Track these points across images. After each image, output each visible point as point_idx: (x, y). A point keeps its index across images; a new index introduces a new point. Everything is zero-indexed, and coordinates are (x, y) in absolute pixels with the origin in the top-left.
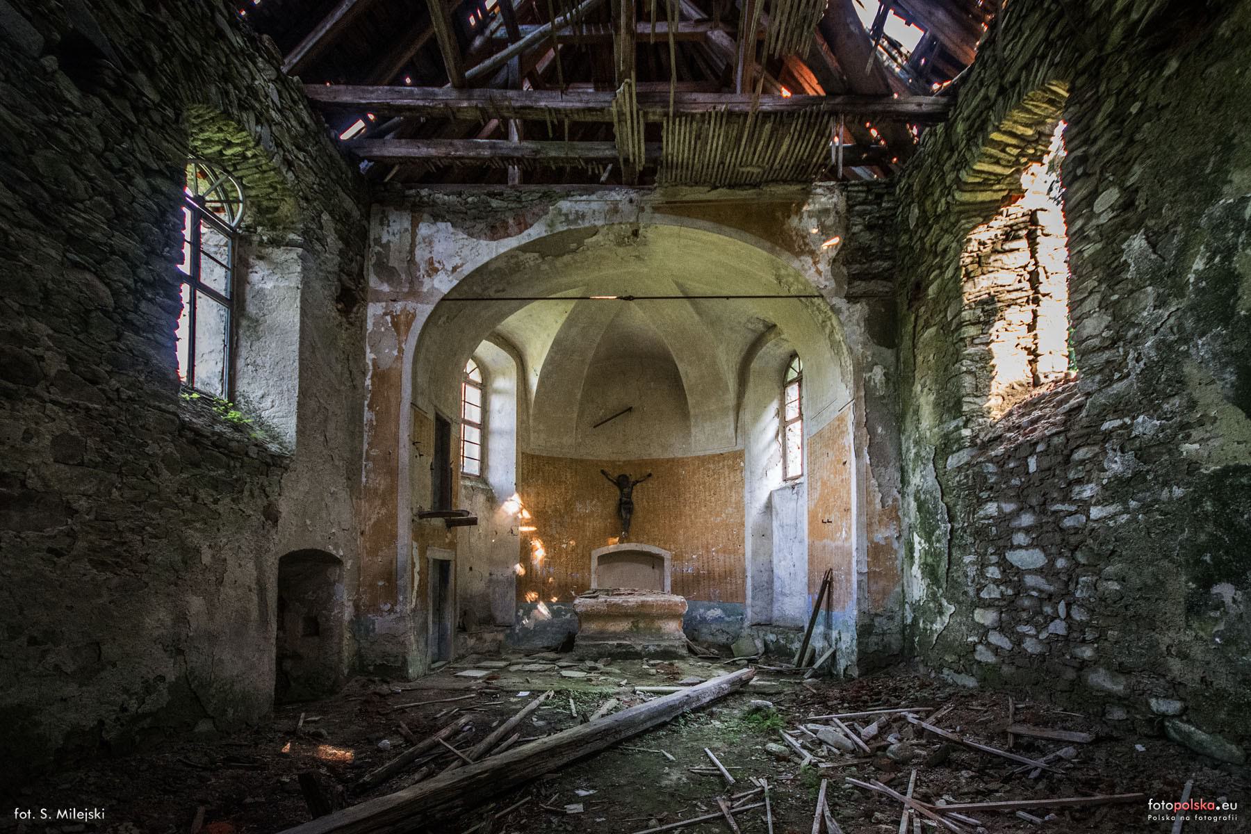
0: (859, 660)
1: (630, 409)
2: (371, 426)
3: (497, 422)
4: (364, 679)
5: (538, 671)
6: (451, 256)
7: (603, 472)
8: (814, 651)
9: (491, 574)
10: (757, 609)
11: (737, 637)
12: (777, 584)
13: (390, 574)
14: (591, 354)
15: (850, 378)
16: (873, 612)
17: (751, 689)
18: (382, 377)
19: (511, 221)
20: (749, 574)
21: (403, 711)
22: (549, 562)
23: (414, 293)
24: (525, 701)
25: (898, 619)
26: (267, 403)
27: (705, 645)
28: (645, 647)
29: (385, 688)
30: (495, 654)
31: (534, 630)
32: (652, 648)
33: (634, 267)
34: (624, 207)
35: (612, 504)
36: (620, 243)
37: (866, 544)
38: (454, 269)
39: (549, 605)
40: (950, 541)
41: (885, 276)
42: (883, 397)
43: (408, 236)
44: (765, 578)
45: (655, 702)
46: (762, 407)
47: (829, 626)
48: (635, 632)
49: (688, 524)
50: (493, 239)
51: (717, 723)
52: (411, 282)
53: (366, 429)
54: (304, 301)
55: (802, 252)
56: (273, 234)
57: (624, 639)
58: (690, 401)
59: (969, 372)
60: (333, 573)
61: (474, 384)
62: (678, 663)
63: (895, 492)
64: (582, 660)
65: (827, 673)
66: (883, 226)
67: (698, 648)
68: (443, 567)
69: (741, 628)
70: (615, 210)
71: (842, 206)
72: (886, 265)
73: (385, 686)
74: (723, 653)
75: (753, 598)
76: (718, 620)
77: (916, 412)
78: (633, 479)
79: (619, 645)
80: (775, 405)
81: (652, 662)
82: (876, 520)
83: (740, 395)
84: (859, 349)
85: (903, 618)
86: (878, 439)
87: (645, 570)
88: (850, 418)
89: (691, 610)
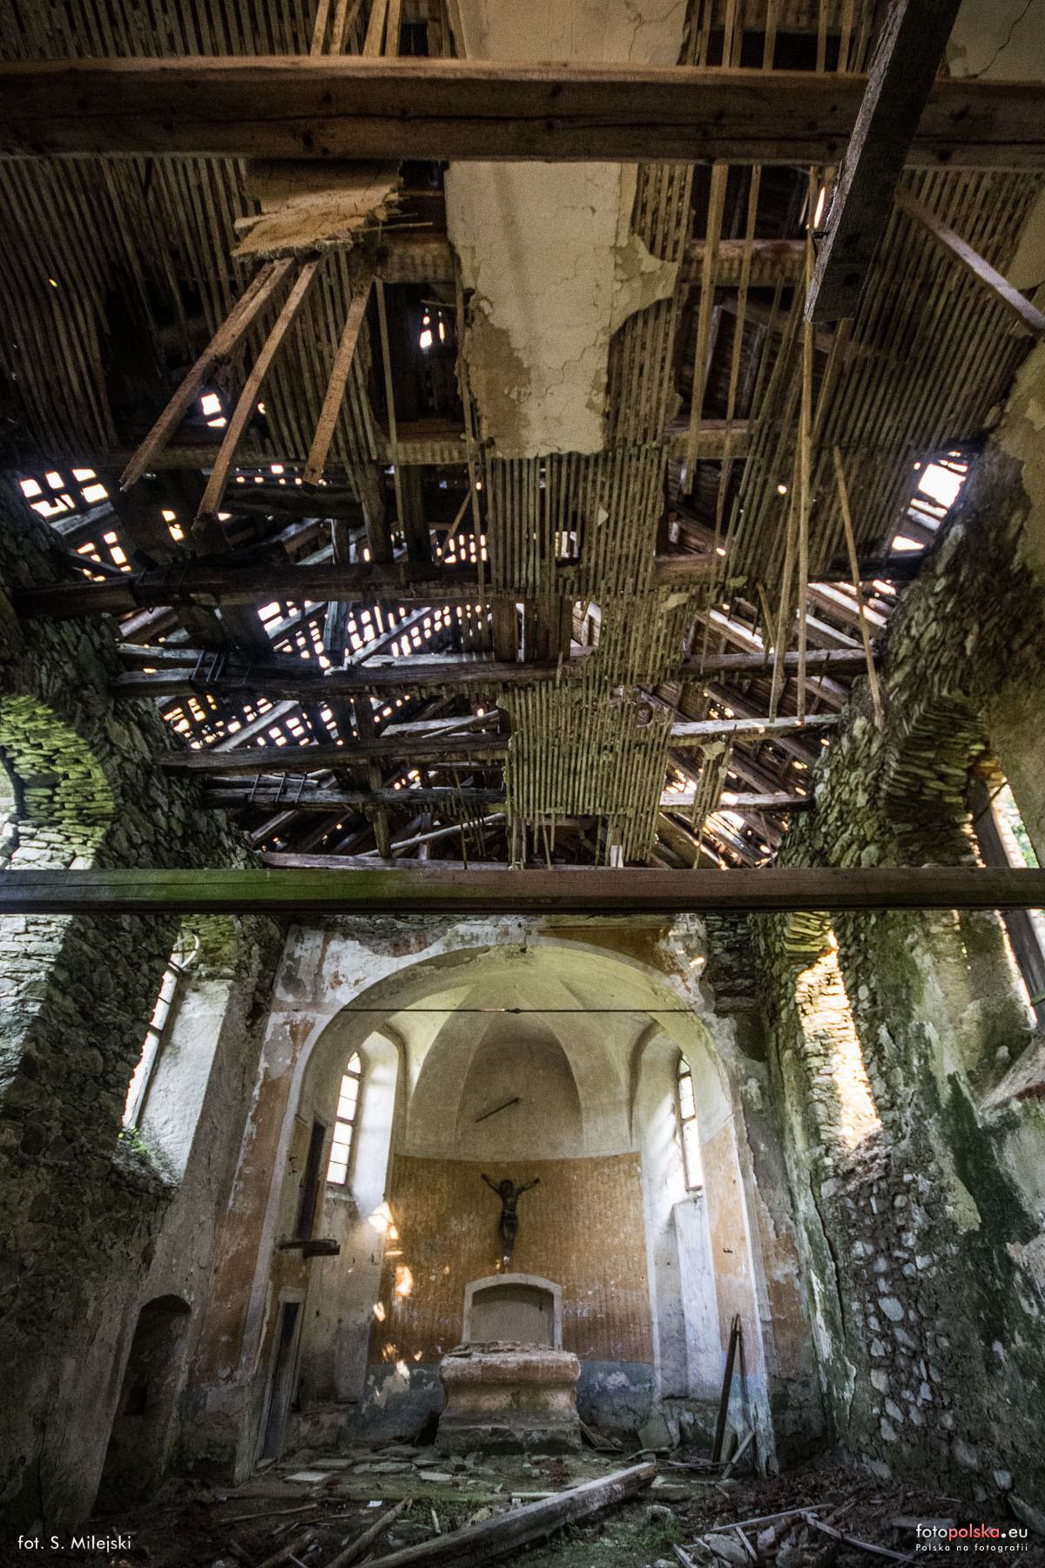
0: (777, 1447)
1: (516, 1100)
2: (251, 1140)
3: (368, 1120)
4: (179, 1481)
5: (392, 1473)
6: (354, 971)
7: (484, 1177)
8: (735, 1436)
9: (340, 1321)
10: (669, 1373)
11: (645, 1419)
12: (690, 1335)
13: (237, 1325)
14: (477, 1043)
15: (727, 1089)
16: (784, 1375)
17: (653, 1494)
18: (273, 1088)
19: (413, 941)
20: (655, 1320)
21: (231, 1526)
22: (413, 1301)
23: (316, 1004)
24: (377, 1513)
25: (813, 1385)
26: (169, 1128)
27: (606, 1432)
28: (528, 1434)
29: (206, 1496)
30: (331, 1449)
31: (386, 1410)
32: (536, 1436)
33: (521, 969)
34: (514, 930)
35: (493, 1218)
36: (510, 955)
37: (765, 1282)
38: (357, 982)
39: (411, 1364)
40: (838, 1282)
41: (748, 993)
42: (761, 1111)
43: (319, 952)
44: (675, 1326)
45: (533, 1508)
46: (655, 1102)
47: (745, 1398)
48: (514, 1410)
49: (582, 1246)
50: (395, 955)
51: (607, 1541)
52: (315, 994)
53: (244, 1143)
54: (224, 1026)
55: (671, 972)
56: (211, 969)
57: (500, 1422)
58: (581, 1092)
59: (821, 1101)
60: (178, 1324)
61: (353, 1075)
62: (569, 1460)
63: (787, 1219)
64: (446, 1456)
65: (747, 1472)
66: (740, 948)
67: (596, 1437)
68: (290, 1313)
69: (651, 1403)
70: (506, 933)
71: (703, 932)
72: (747, 983)
73: (205, 1492)
74: (626, 1445)
75: (663, 1356)
76: (622, 1389)
77: (791, 1130)
78: (517, 1186)
79: (495, 1432)
80: (669, 1100)
81: (535, 1458)
82: (772, 1252)
83: (633, 1087)
84: (732, 1061)
85: (820, 1385)
86: (762, 1158)
87: (529, 1313)
88: (733, 1133)
89: (587, 1374)
